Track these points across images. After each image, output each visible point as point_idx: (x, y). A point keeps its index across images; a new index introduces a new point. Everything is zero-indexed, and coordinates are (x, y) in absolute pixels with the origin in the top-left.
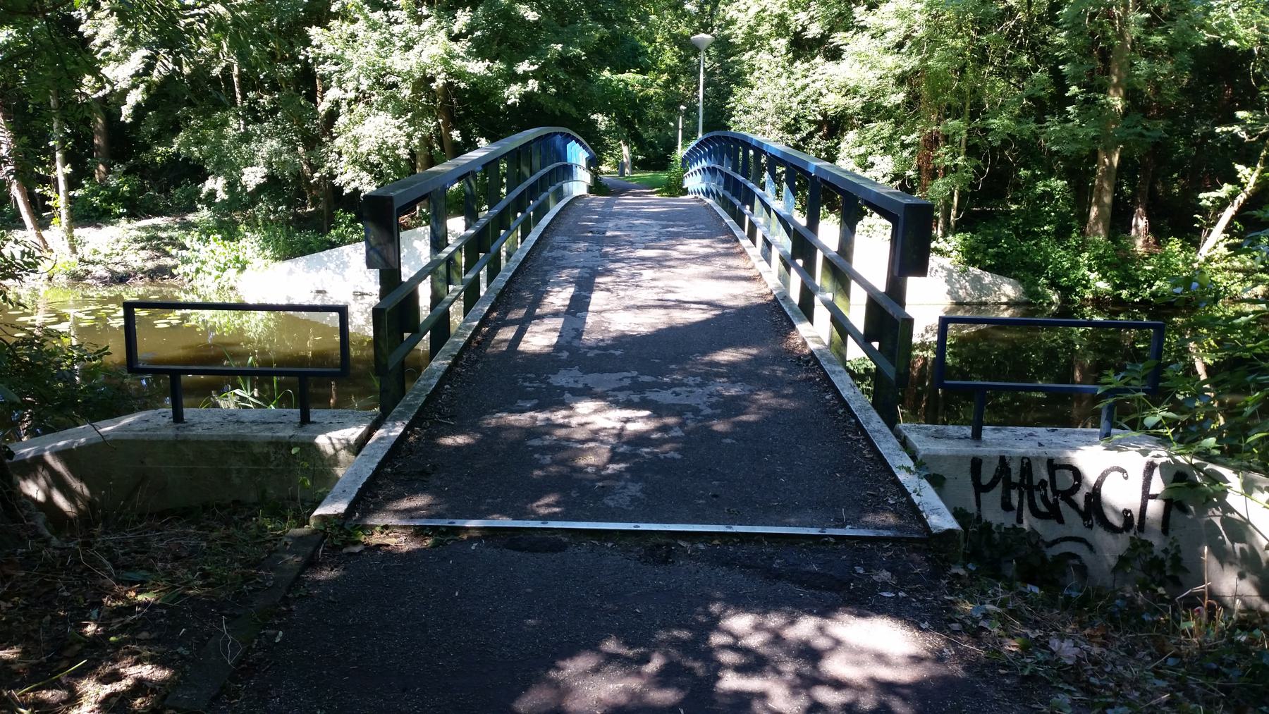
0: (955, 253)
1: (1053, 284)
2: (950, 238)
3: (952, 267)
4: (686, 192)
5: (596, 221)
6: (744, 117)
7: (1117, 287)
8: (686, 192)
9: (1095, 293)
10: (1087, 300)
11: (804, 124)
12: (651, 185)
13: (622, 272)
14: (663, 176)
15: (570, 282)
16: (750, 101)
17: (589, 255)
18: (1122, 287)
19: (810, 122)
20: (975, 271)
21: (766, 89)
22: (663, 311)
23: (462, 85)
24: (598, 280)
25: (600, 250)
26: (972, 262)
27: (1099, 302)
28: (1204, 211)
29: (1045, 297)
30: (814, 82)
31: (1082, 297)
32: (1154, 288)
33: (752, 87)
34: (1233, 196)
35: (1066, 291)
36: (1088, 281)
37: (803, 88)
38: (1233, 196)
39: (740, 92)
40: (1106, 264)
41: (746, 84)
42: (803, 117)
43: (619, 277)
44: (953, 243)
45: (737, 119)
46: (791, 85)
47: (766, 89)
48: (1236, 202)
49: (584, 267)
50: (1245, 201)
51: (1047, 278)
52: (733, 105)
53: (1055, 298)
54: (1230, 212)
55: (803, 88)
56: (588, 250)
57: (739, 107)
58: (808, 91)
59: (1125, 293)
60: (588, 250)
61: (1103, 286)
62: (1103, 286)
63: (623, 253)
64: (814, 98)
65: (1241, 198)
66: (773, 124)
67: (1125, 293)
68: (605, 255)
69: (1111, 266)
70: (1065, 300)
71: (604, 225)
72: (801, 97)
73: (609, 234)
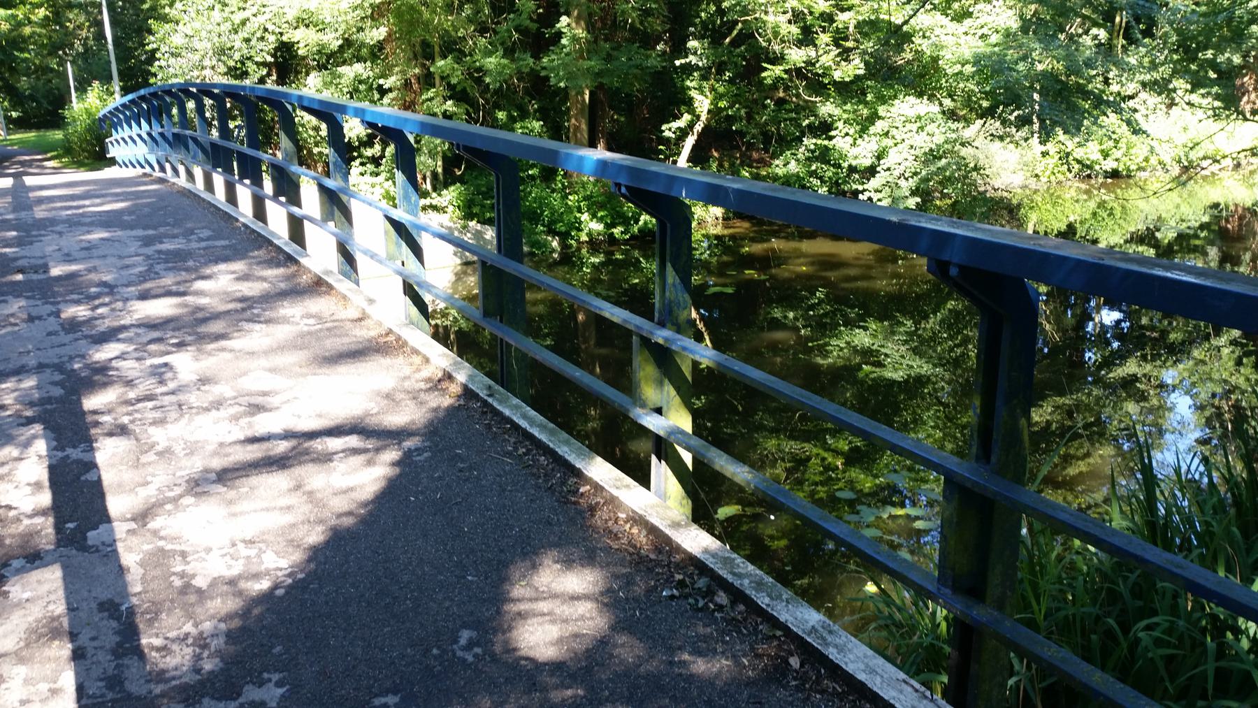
0: (451, 208)
1: (552, 232)
2: (445, 192)
3: (451, 224)
4: (112, 162)
5: (19, 242)
6: (172, 61)
7: (609, 226)
8: (112, 162)
9: (589, 234)
10: (583, 243)
11: (251, 67)
12: (42, 148)
13: (129, 367)
14: (58, 135)
15: (29, 421)
16: (177, 40)
17: (38, 329)
18: (613, 225)
19: (258, 64)
20: (473, 224)
21: (197, 25)
22: (277, 481)
23: (1155, 334)
24: (91, 402)
25: (57, 314)
26: (469, 216)
27: (594, 245)
28: (667, 141)
29: (545, 244)
30: (254, 15)
31: (578, 241)
32: (641, 223)
33: (177, 23)
34: (691, 126)
35: (564, 236)
36: (580, 223)
37: (244, 23)
38: (691, 126)
39: (161, 29)
40: (595, 203)
41: (165, 19)
42: (248, 59)
43: (129, 383)
44: (449, 198)
45: (163, 63)
46: (226, 20)
47: (197, 25)
48: (695, 131)
49: (41, 367)
50: (703, 129)
51: (543, 225)
52: (155, 46)
53: (555, 244)
54: (690, 141)
55: (244, 23)
56: (31, 319)
57: (163, 49)
58: (249, 27)
59: (617, 231)
60: (31, 319)
61: (597, 227)
62: (597, 227)
63: (106, 315)
64: (259, 35)
65: (698, 127)
66: (213, 68)
67: (617, 231)
68: (73, 326)
69: (602, 206)
70: (565, 246)
71: (34, 250)
72: (243, 34)
73: (56, 271)
